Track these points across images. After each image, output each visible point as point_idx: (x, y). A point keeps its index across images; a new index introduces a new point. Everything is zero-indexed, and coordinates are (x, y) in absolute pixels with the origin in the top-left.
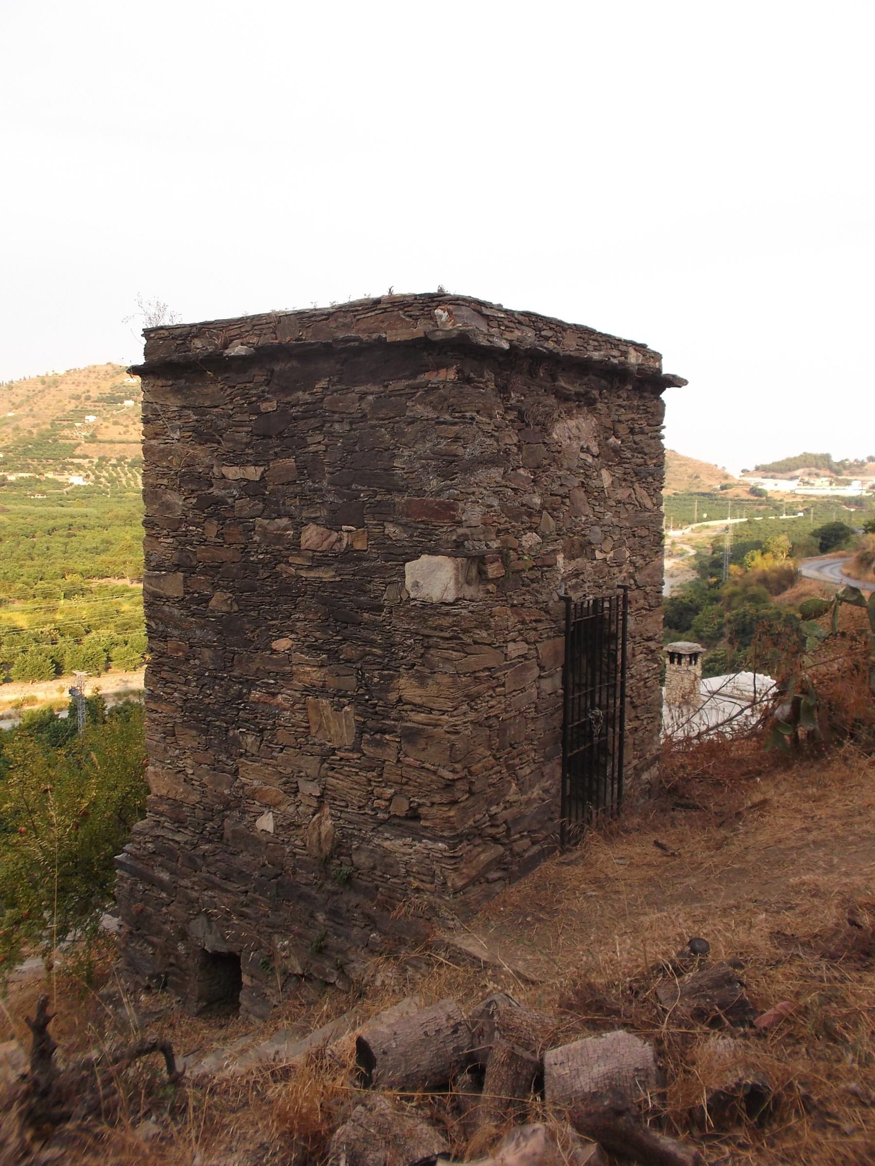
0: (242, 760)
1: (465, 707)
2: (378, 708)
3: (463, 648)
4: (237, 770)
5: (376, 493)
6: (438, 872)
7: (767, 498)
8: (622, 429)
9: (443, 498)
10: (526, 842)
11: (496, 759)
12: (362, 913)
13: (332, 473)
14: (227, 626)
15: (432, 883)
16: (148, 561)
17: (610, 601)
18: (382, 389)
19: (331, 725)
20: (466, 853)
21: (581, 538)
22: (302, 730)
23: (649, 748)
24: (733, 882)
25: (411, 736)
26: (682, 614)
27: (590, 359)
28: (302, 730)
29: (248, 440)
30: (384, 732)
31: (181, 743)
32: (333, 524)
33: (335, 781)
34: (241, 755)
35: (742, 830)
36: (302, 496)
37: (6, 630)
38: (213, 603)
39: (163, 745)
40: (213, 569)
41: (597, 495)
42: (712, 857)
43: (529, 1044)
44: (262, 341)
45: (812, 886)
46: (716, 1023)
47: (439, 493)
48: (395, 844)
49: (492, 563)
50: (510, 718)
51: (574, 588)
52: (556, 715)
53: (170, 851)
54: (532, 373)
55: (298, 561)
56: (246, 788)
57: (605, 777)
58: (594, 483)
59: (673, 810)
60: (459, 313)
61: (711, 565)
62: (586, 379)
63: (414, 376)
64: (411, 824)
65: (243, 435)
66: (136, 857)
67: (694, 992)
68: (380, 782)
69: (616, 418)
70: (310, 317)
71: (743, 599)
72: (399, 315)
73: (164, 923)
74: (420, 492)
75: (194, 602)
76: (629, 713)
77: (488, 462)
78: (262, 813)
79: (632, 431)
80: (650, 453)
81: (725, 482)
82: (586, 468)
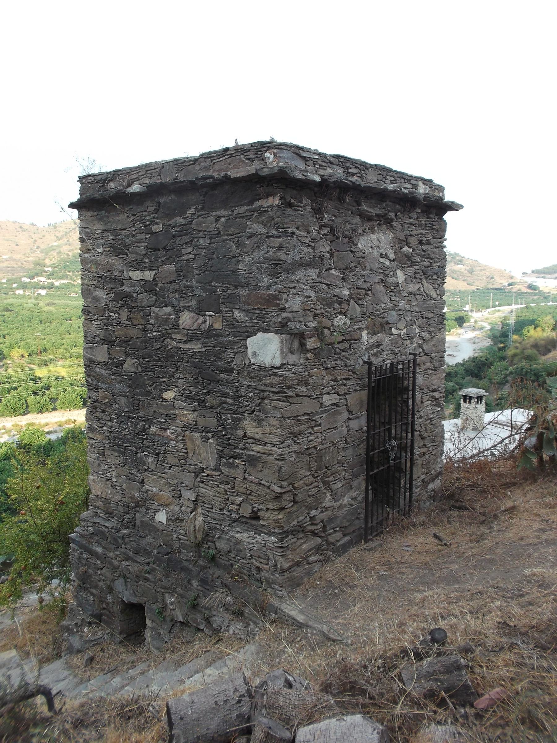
0: (146, 473)
1: (289, 441)
2: (230, 441)
3: (287, 399)
4: (143, 480)
5: (227, 288)
6: (271, 557)
7: (540, 291)
8: (413, 241)
9: (272, 291)
10: (339, 535)
11: (315, 478)
12: (222, 583)
13: (198, 275)
14: (134, 382)
15: (267, 564)
16: (86, 337)
17: (403, 364)
18: (230, 213)
19: (201, 451)
20: (292, 544)
21: (380, 320)
22: (183, 454)
23: (433, 466)
24: (484, 569)
25: (252, 461)
26: (480, 368)
27: (385, 189)
28: (183, 454)
29: (145, 252)
30: (235, 458)
31: (109, 460)
32: (200, 311)
33: (204, 490)
34: (145, 470)
35: (496, 528)
36: (179, 291)
37: (54, 378)
38: (125, 366)
39: (98, 462)
40: (126, 342)
41: (394, 289)
42: (472, 548)
43: (290, 719)
44: (152, 181)
45: (540, 577)
46: (442, 703)
47: (268, 288)
48: (243, 536)
49: (310, 338)
50: (326, 448)
51: (376, 355)
52: (362, 445)
53: (103, 533)
54: (341, 200)
55: (178, 337)
56: (149, 492)
57: (400, 487)
58: (391, 280)
59: (450, 510)
60: (282, 155)
61: (501, 336)
62: (384, 205)
63: (251, 203)
64: (254, 522)
65: (142, 250)
66: (82, 536)
67: (430, 676)
68: (233, 492)
69: (408, 233)
70: (183, 163)
71: (521, 358)
72: (241, 158)
73: (99, 581)
74: (257, 287)
75: (115, 365)
76: (418, 442)
77: (306, 265)
78: (159, 510)
79: (421, 242)
80: (434, 258)
81: (511, 281)
82: (384, 269)
